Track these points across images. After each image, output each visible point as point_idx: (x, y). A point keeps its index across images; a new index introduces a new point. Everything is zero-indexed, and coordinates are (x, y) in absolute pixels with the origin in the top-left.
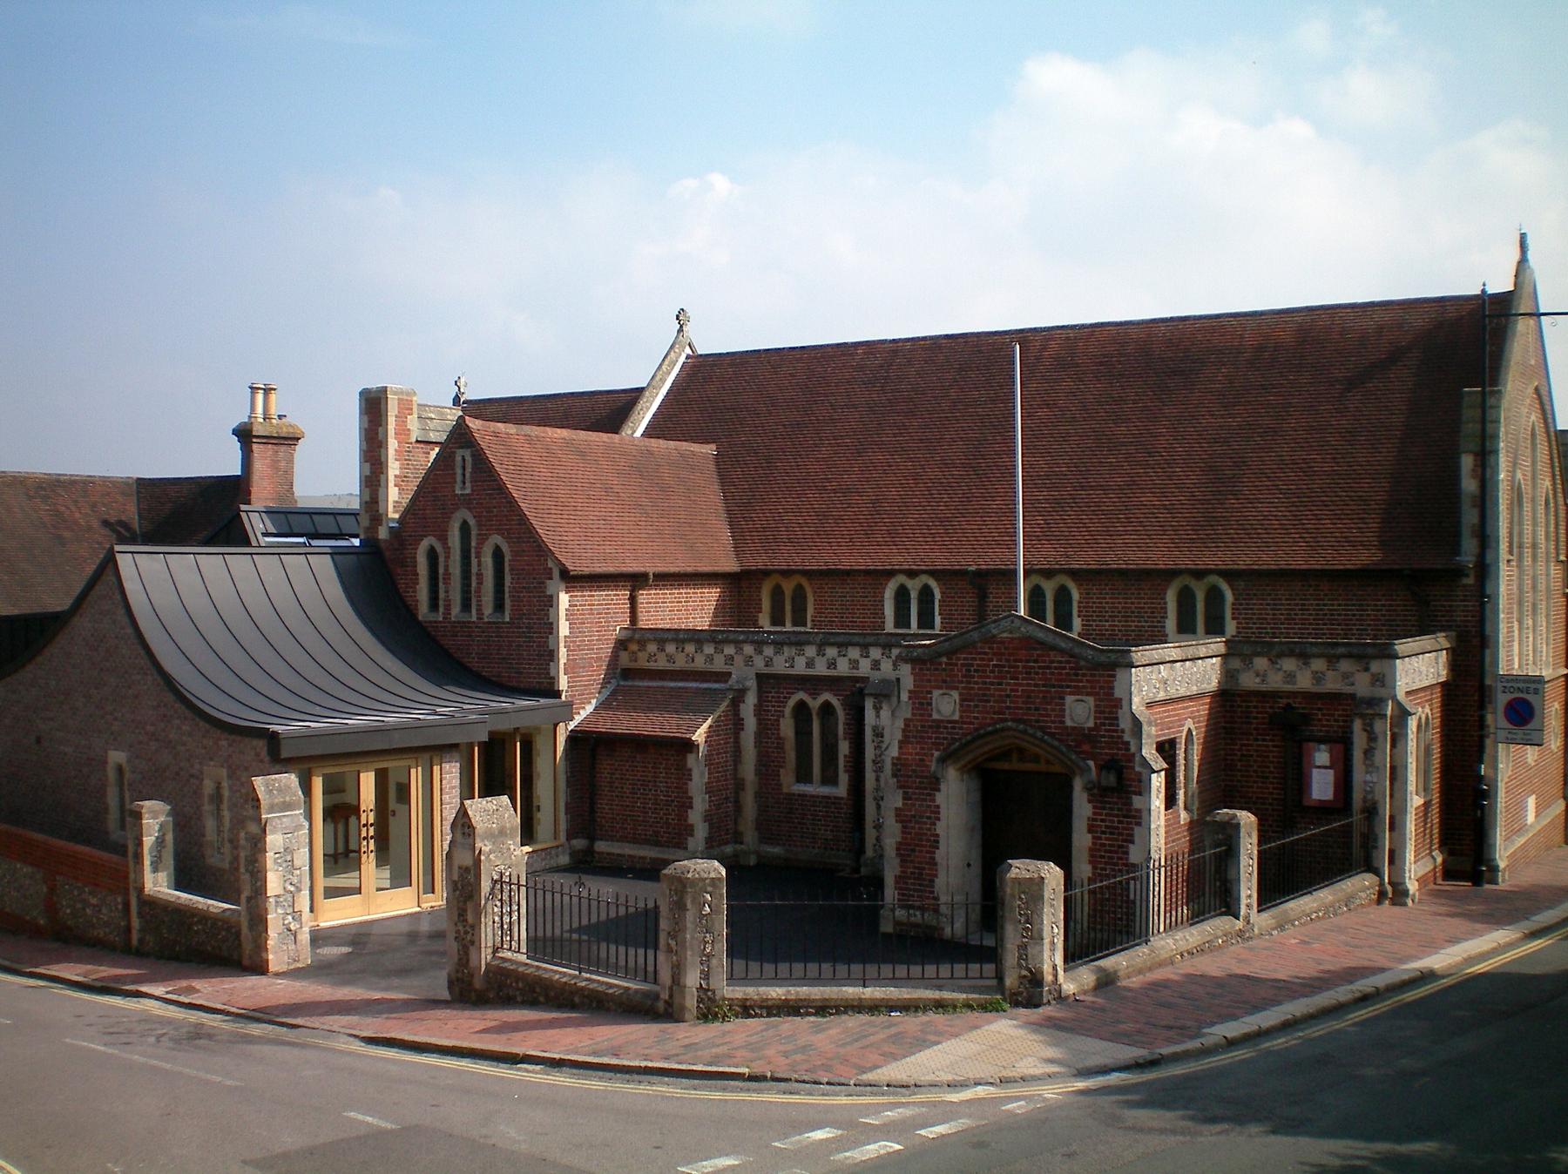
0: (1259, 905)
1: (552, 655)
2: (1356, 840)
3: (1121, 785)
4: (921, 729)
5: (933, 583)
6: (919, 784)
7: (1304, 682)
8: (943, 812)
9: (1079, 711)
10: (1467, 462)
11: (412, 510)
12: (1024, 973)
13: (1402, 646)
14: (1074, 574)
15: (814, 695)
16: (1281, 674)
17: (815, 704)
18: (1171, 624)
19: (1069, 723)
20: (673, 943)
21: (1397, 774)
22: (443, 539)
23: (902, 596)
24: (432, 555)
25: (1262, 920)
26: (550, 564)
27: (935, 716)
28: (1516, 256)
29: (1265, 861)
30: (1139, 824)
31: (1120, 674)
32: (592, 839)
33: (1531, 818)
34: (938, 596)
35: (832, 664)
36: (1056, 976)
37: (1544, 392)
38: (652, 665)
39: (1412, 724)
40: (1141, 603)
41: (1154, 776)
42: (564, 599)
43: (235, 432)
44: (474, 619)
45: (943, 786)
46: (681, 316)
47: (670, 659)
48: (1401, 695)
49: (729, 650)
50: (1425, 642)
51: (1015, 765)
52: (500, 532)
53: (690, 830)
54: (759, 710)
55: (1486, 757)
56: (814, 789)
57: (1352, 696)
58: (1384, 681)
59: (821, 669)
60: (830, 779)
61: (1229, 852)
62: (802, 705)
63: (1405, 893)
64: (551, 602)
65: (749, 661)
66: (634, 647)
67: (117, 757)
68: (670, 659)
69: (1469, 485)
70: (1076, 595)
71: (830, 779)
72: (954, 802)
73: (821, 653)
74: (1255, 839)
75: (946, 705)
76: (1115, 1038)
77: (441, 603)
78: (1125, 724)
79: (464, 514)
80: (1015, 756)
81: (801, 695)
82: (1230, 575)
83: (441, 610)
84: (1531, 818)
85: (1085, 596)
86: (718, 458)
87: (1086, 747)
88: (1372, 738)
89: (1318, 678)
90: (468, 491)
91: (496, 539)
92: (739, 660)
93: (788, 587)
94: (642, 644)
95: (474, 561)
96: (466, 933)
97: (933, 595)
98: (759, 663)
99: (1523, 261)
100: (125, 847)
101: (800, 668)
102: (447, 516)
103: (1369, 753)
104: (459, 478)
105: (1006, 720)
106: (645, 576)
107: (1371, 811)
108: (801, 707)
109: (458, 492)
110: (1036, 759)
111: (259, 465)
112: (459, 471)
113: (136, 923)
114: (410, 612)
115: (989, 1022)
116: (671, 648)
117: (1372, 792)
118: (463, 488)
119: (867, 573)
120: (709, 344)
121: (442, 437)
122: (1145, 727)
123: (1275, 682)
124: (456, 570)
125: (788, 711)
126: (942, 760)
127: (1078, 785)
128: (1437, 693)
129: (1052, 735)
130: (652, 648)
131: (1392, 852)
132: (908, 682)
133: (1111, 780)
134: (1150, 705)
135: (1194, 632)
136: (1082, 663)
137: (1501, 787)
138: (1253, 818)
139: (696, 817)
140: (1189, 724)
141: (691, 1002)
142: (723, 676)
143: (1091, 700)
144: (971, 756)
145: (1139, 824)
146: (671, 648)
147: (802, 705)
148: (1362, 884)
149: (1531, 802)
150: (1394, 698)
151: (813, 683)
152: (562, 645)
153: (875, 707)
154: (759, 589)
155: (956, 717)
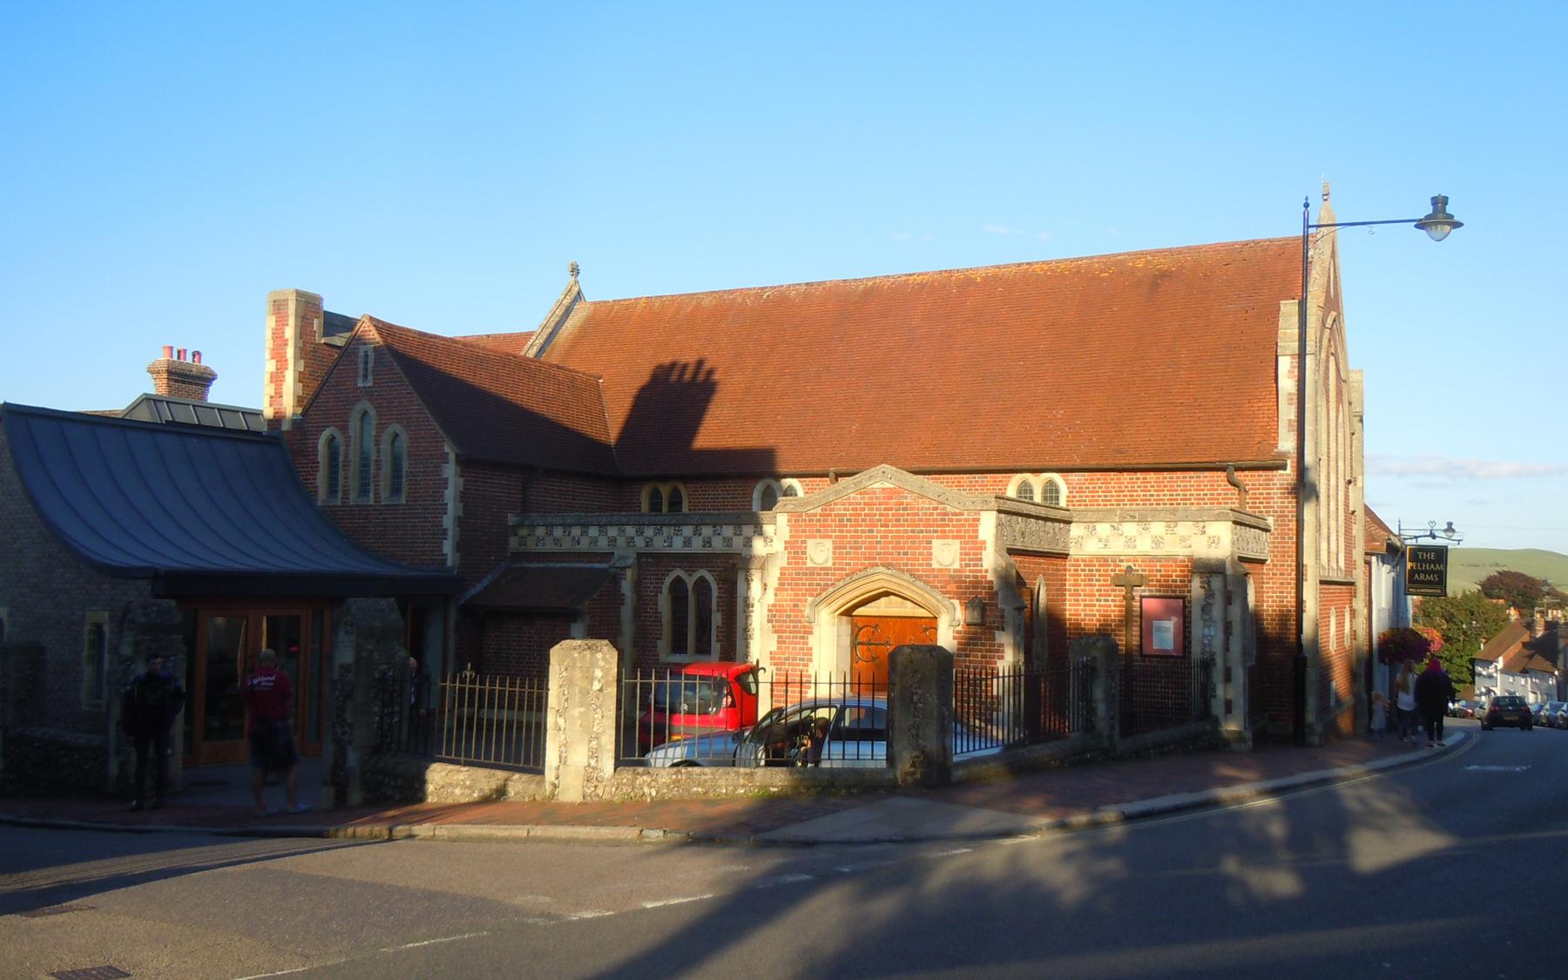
7: (1144, 546)
8: (815, 656)
16: (1122, 539)
17: (690, 581)
19: (935, 565)
22: (344, 428)
27: (809, 564)
35: (708, 542)
38: (540, 548)
44: (372, 502)
45: (816, 630)
46: (575, 271)
54: (638, 585)
59: (697, 546)
62: (678, 581)
65: (631, 540)
68: (557, 541)
73: (697, 533)
77: (340, 488)
79: (365, 405)
81: (679, 572)
83: (340, 495)
89: (1157, 542)
90: (370, 384)
91: (396, 427)
92: (621, 541)
96: (344, 733)
98: (640, 542)
101: (678, 546)
104: (361, 372)
107: (1207, 665)
108: (678, 584)
109: (360, 385)
112: (361, 366)
114: (309, 497)
117: (1210, 645)
123: (1117, 547)
136: (949, 509)
142: (606, 556)
143: (957, 542)
147: (678, 580)
151: (690, 561)
155: (829, 564)
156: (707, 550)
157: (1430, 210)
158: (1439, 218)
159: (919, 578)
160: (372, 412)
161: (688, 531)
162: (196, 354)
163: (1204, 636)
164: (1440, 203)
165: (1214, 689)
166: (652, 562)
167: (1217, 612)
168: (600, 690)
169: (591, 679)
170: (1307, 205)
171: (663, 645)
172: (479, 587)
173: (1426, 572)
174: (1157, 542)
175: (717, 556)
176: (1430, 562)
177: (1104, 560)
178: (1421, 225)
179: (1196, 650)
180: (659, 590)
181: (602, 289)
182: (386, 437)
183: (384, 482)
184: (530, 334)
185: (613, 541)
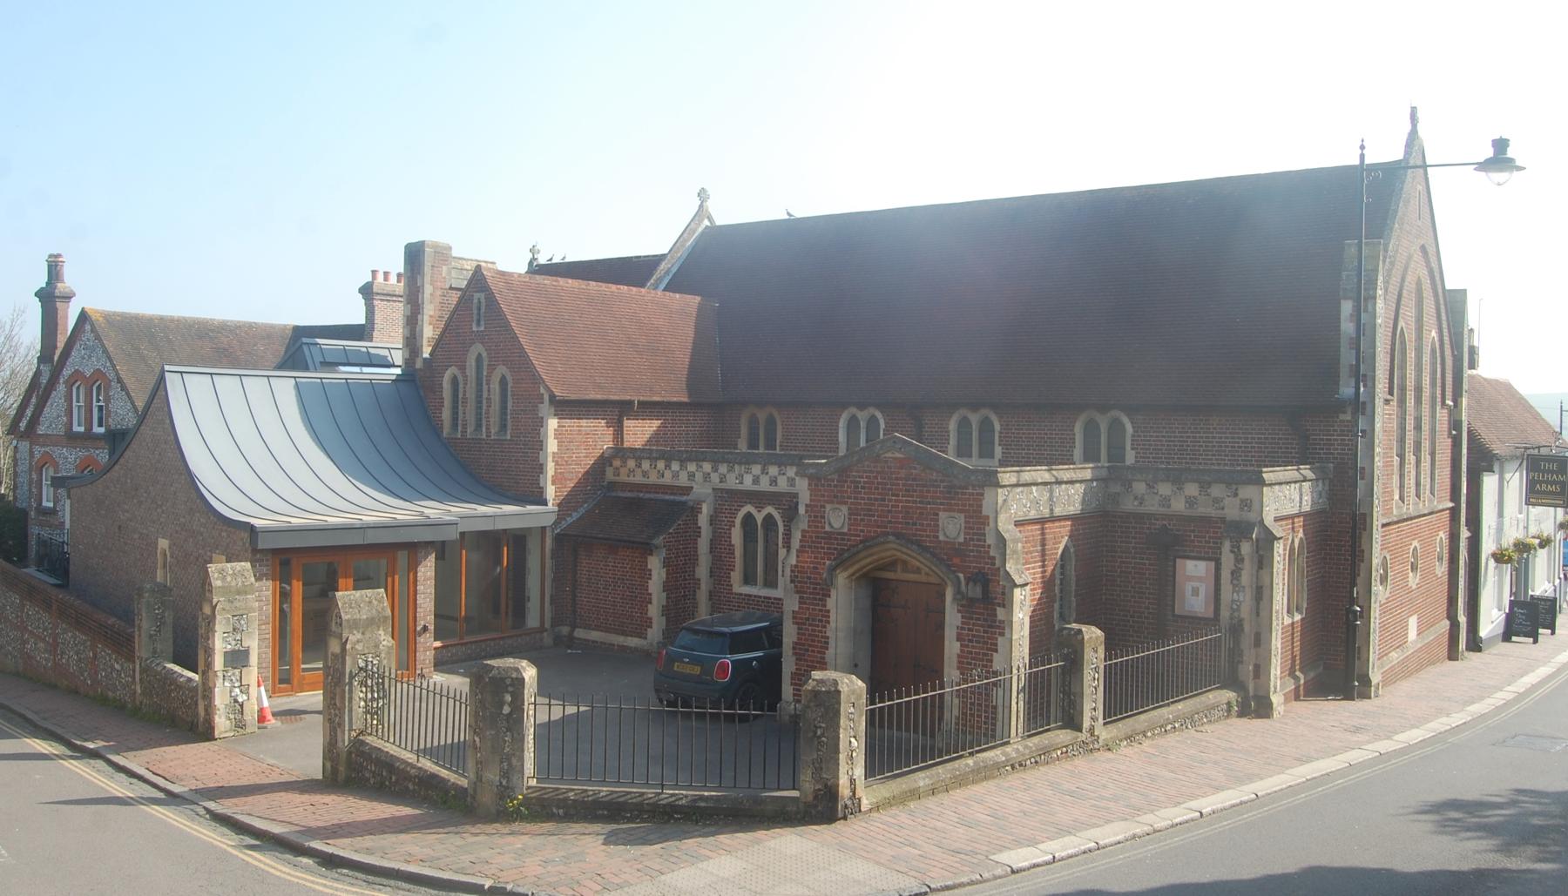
1: (541, 468)
4: (819, 538)
5: (879, 415)
6: (814, 590)
7: (1179, 506)
9: (951, 527)
10: (1347, 307)
11: (438, 345)
13: (1269, 475)
15: (760, 508)
17: (759, 518)
18: (1078, 452)
22: (463, 368)
25: (1104, 733)
26: (542, 390)
27: (827, 528)
28: (1408, 127)
29: (1112, 678)
30: (1002, 634)
31: (988, 492)
32: (574, 627)
33: (1412, 634)
35: (774, 482)
38: (631, 479)
42: (553, 423)
45: (833, 593)
46: (703, 195)
47: (645, 474)
48: (1268, 520)
49: (692, 467)
50: (1289, 473)
51: (899, 575)
53: (648, 623)
54: (713, 520)
55: (1359, 580)
57: (1223, 520)
59: (765, 485)
61: (1074, 664)
62: (749, 516)
64: (540, 423)
65: (707, 477)
66: (617, 463)
67: (163, 543)
68: (645, 474)
69: (1347, 327)
73: (668, 466)
75: (837, 519)
78: (990, 540)
80: (899, 568)
81: (749, 508)
84: (1412, 634)
87: (956, 561)
89: (1191, 502)
91: (502, 370)
92: (699, 476)
95: (485, 387)
98: (715, 478)
99: (1413, 136)
103: (1236, 574)
106: (631, 403)
107: (1236, 629)
108: (749, 520)
110: (918, 571)
114: (436, 430)
115: (697, 858)
117: (1238, 610)
118: (478, 324)
121: (463, 284)
123: (1152, 506)
124: (471, 395)
125: (738, 521)
126: (833, 570)
128: (1299, 522)
130: (631, 463)
133: (976, 591)
134: (1018, 524)
137: (1375, 613)
138: (1099, 632)
139: (654, 611)
144: (856, 567)
145: (1002, 634)
147: (749, 516)
149: (1413, 622)
151: (759, 498)
152: (550, 459)
156: (773, 489)
158: (1499, 159)
160: (484, 354)
161: (756, 469)
163: (1233, 601)
164: (1501, 145)
165: (1241, 655)
166: (729, 499)
167: (1246, 578)
168: (510, 714)
169: (501, 704)
170: (1362, 147)
171: (736, 576)
173: (1547, 482)
174: (1191, 502)
176: (1553, 472)
177: (1140, 517)
179: (1225, 614)
181: (731, 211)
183: (494, 419)
185: (691, 476)
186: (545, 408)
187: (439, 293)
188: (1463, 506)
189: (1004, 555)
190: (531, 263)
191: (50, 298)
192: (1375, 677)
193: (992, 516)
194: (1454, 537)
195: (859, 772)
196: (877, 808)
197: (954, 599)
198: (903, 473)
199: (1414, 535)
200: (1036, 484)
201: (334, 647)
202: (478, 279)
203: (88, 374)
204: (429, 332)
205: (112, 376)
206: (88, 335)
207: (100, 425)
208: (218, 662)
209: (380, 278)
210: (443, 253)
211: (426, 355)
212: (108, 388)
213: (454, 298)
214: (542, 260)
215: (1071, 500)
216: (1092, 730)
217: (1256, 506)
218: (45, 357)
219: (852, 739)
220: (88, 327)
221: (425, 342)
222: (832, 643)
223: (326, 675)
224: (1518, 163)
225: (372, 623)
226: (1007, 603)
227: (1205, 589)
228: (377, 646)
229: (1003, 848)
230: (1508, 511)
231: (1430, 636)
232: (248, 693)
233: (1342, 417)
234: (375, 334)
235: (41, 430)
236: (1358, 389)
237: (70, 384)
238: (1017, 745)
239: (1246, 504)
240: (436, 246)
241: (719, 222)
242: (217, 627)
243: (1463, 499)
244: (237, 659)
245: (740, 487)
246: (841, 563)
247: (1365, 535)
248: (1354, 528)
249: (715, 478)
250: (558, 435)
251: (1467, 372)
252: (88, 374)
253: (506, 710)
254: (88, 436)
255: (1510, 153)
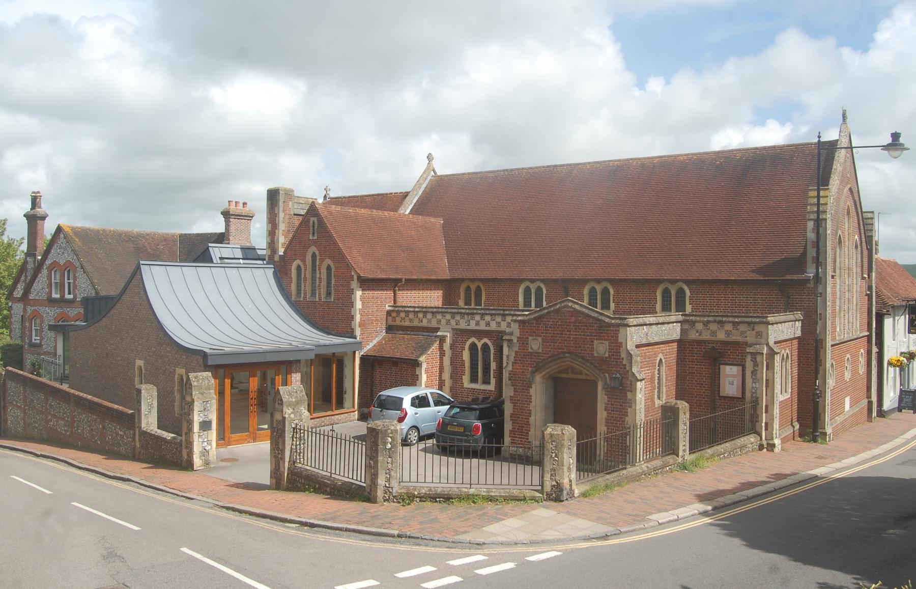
0: (691, 449)
1: (352, 318)
2: (747, 416)
3: (622, 388)
4: (522, 356)
5: (542, 286)
6: (522, 385)
7: (721, 336)
9: (601, 348)
11: (288, 248)
12: (554, 483)
14: (611, 281)
15: (479, 340)
17: (479, 345)
18: (659, 306)
20: (372, 462)
21: (770, 384)
22: (304, 261)
23: (527, 292)
24: (299, 268)
27: (530, 350)
30: (631, 407)
31: (622, 330)
33: (847, 407)
34: (545, 292)
35: (488, 324)
36: (571, 485)
37: (855, 191)
38: (403, 324)
39: (777, 358)
40: (639, 294)
41: (638, 383)
42: (359, 293)
43: (222, 213)
45: (534, 386)
46: (430, 157)
48: (771, 343)
49: (439, 317)
50: (789, 316)
52: (329, 258)
54: (452, 346)
56: (479, 386)
58: (762, 336)
59: (482, 327)
60: (486, 381)
63: (774, 445)
64: (352, 292)
66: (394, 314)
67: (140, 363)
68: (411, 321)
70: (612, 292)
71: (486, 381)
72: (538, 394)
73: (482, 318)
74: (688, 416)
75: (535, 345)
76: (598, 520)
78: (623, 355)
79: (313, 249)
81: (473, 339)
82: (688, 282)
84: (847, 407)
85: (617, 292)
86: (444, 226)
87: (604, 367)
88: (756, 365)
91: (328, 262)
92: (443, 322)
93: (473, 287)
94: (398, 312)
95: (318, 272)
97: (685, 294)
98: (453, 322)
100: (342, 407)
101: (473, 326)
102: (306, 249)
103: (754, 373)
105: (565, 353)
106: (401, 280)
107: (756, 402)
110: (581, 373)
111: (232, 228)
112: (311, 228)
113: (138, 445)
116: (429, 316)
117: (756, 392)
119: (512, 280)
120: (442, 171)
122: (634, 358)
125: (467, 347)
126: (533, 373)
127: (600, 387)
128: (795, 342)
129: (587, 360)
131: (766, 424)
132: (517, 333)
134: (637, 346)
135: (670, 311)
140: (661, 356)
141: (380, 493)
146: (429, 316)
148: (751, 440)
149: (847, 401)
150: (768, 345)
151: (479, 334)
153: (509, 346)
154: (459, 288)
156: (487, 328)
157: (890, 140)
159: (587, 360)
160: (317, 253)
162: (245, 204)
164: (896, 136)
171: (466, 378)
172: (371, 345)
175: (493, 332)
177: (699, 342)
178: (886, 147)
179: (748, 394)
180: (463, 349)
182: (324, 266)
183: (323, 290)
184: (405, 195)
185: (439, 322)
186: (354, 284)
187: (287, 217)
188: (874, 334)
189: (631, 363)
190: (325, 197)
191: (34, 220)
192: (829, 430)
193: (624, 342)
194: (869, 352)
195: (573, 476)
196: (584, 495)
197: (603, 388)
198: (573, 319)
199: (847, 351)
200: (646, 325)
201: (277, 416)
202: (313, 209)
203: (62, 263)
204: (282, 240)
205: (77, 264)
206: (61, 240)
207: (69, 293)
208: (196, 427)
209: (233, 206)
210: (289, 193)
211: (281, 253)
212: (75, 271)
213: (297, 221)
214: (332, 195)
215: (674, 331)
216: (683, 456)
217: (764, 335)
218: (31, 252)
219: (569, 458)
220: (62, 236)
221: (280, 245)
222: (533, 413)
223: (272, 433)
224: (905, 146)
225: (298, 403)
226: (633, 390)
227: (737, 381)
228: (301, 415)
229: (651, 514)
230: (898, 337)
231: (857, 409)
232: (210, 444)
233: (808, 285)
234: (231, 238)
235: (32, 297)
236: (817, 270)
237: (50, 269)
238: (641, 466)
239: (759, 334)
240: (285, 190)
241: (439, 174)
242: (195, 408)
243: (874, 330)
244: (205, 426)
245: (468, 328)
246: (538, 369)
247: (822, 351)
248: (817, 347)
249: (453, 322)
250: (362, 299)
251: (875, 257)
252: (62, 263)
253: (389, 446)
254: (62, 301)
255: (901, 140)
